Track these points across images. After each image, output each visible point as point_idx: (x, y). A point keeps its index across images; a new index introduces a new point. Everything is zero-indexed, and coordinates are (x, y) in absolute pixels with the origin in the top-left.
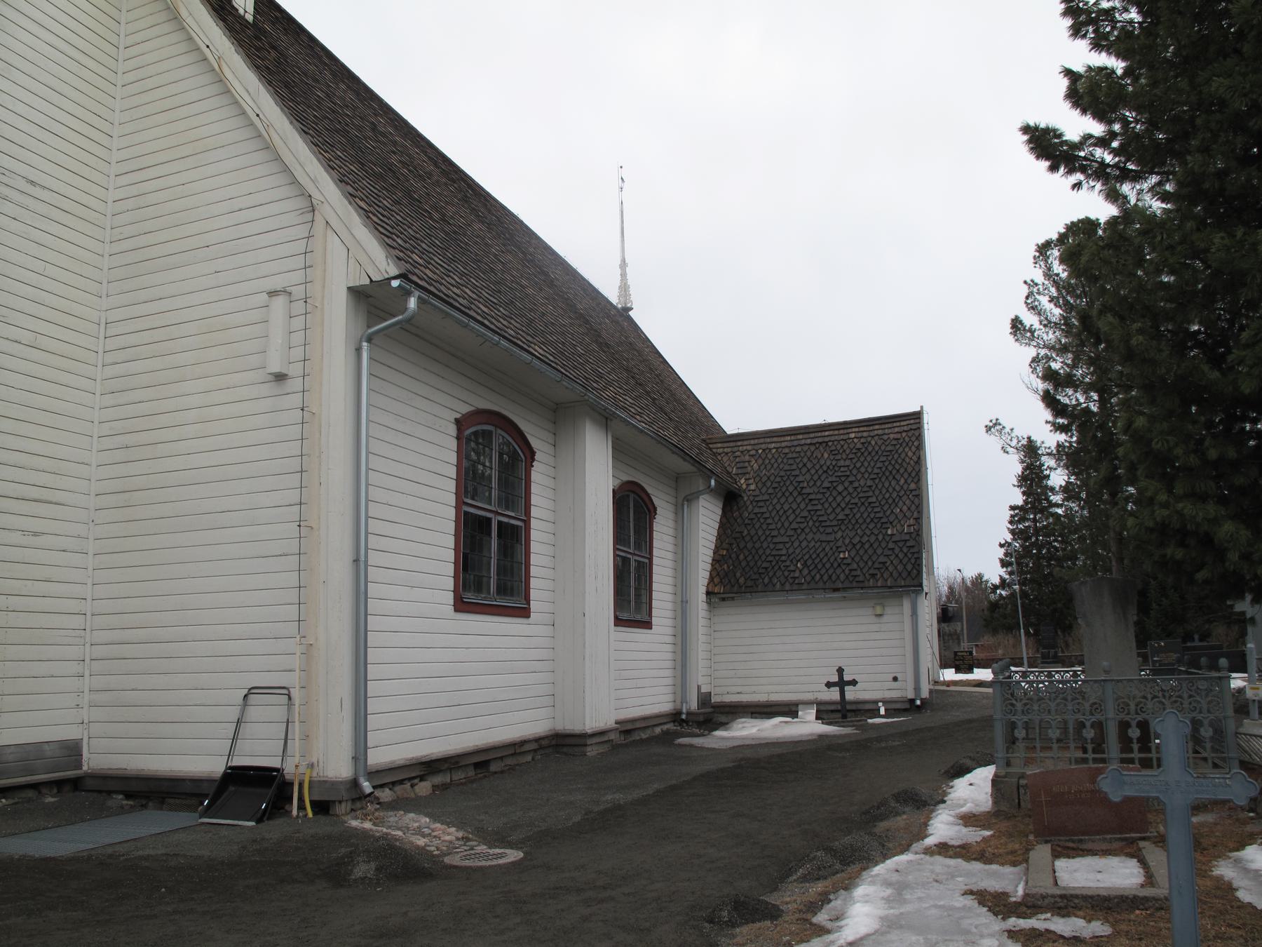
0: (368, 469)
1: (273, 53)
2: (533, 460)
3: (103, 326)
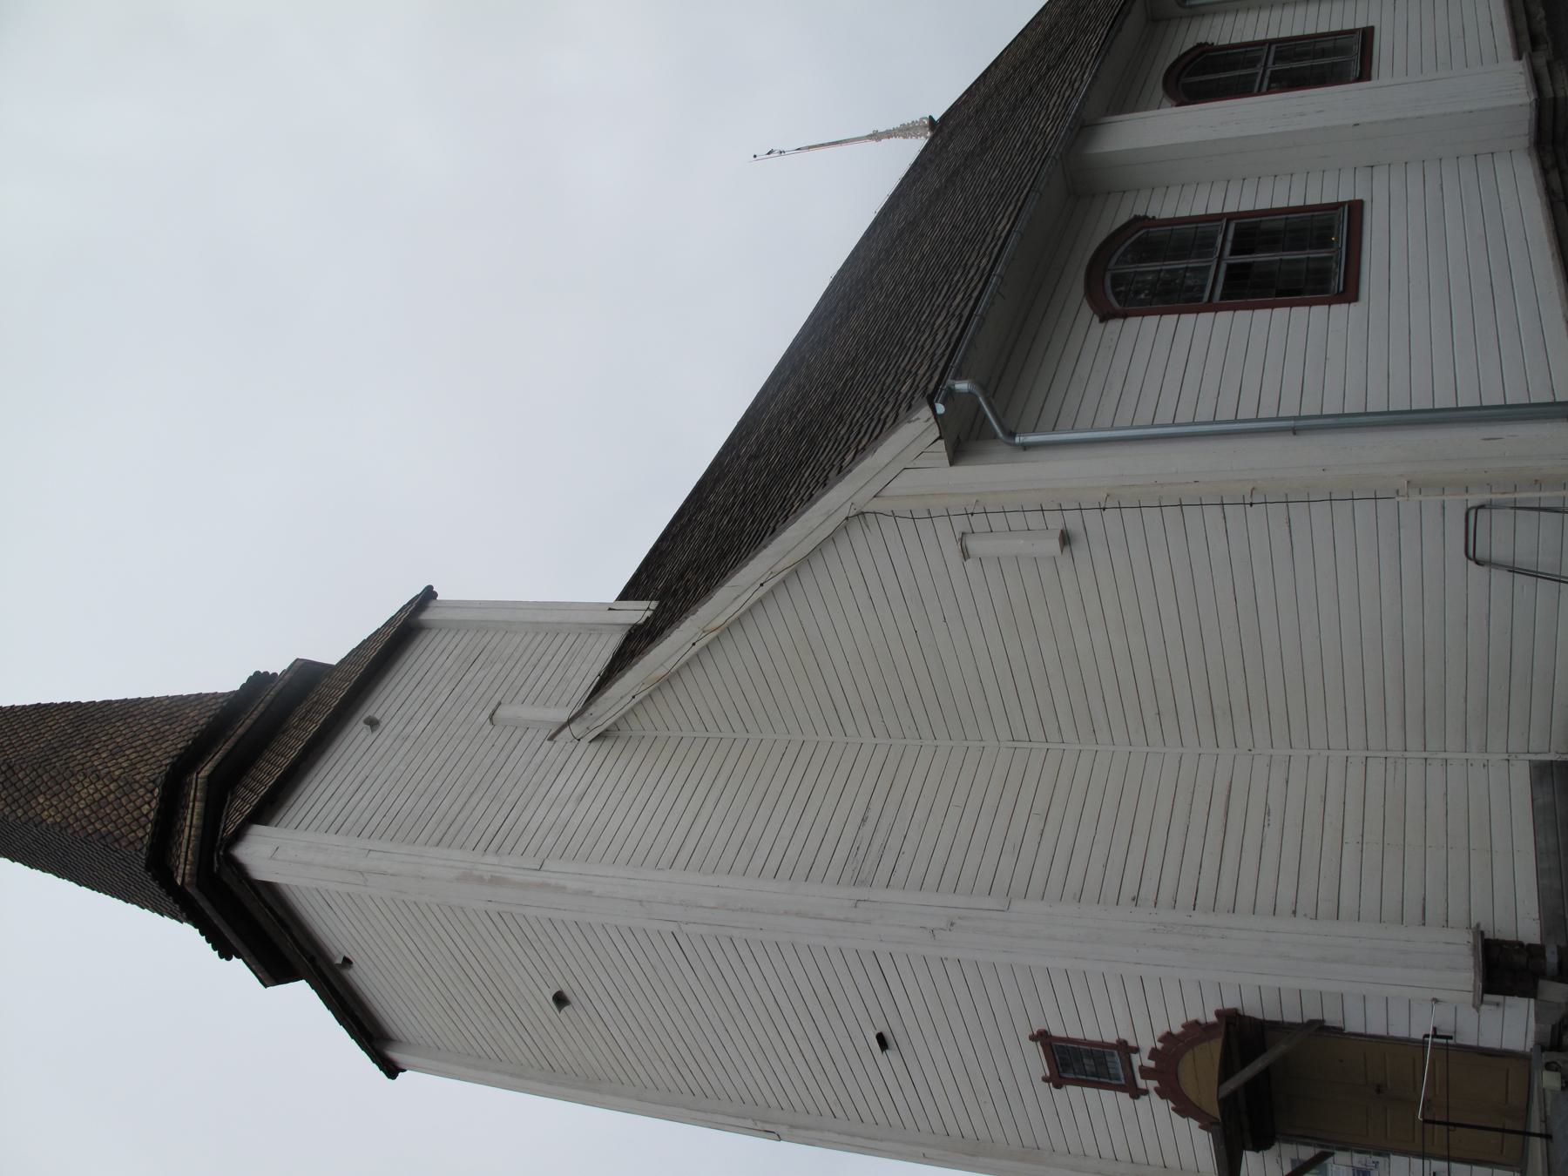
0: (1174, 424)
1: (689, 575)
2: (1145, 217)
3: (1016, 744)
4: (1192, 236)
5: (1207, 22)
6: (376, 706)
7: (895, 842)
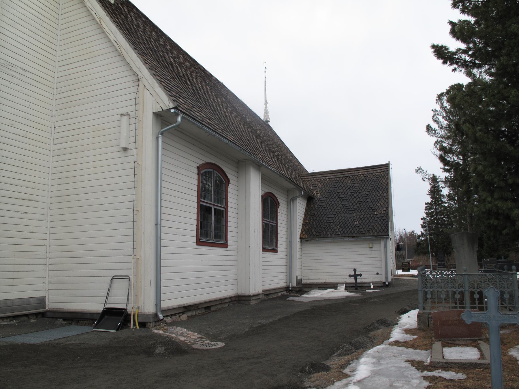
1: (122, 16)
2: (229, 183)
3: (53, 128)
4: (221, 195)
5: (286, 206)
7: (15, 80)
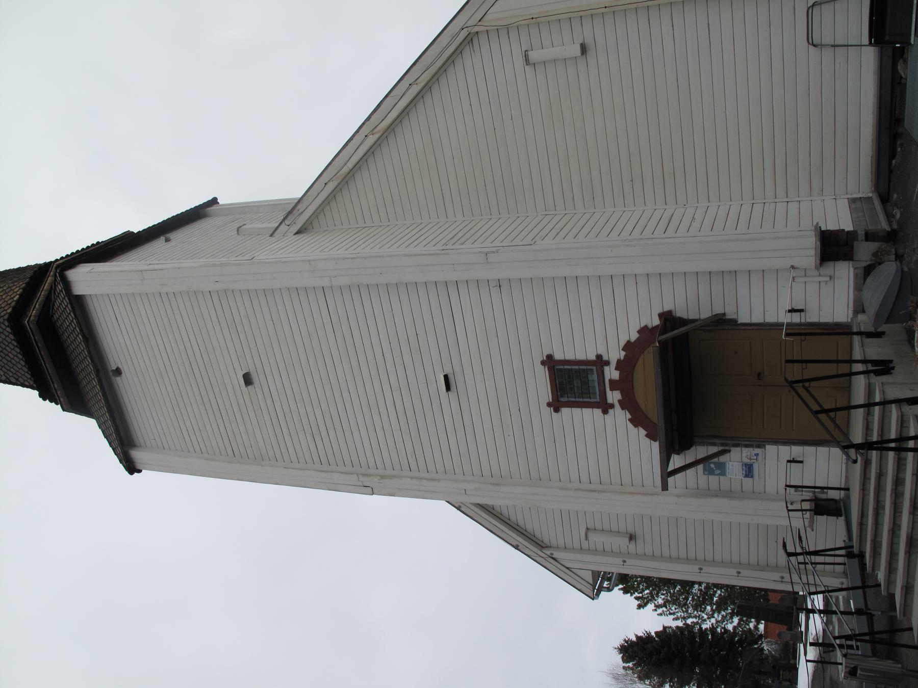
6: (172, 235)
